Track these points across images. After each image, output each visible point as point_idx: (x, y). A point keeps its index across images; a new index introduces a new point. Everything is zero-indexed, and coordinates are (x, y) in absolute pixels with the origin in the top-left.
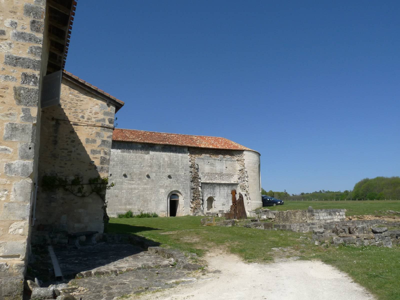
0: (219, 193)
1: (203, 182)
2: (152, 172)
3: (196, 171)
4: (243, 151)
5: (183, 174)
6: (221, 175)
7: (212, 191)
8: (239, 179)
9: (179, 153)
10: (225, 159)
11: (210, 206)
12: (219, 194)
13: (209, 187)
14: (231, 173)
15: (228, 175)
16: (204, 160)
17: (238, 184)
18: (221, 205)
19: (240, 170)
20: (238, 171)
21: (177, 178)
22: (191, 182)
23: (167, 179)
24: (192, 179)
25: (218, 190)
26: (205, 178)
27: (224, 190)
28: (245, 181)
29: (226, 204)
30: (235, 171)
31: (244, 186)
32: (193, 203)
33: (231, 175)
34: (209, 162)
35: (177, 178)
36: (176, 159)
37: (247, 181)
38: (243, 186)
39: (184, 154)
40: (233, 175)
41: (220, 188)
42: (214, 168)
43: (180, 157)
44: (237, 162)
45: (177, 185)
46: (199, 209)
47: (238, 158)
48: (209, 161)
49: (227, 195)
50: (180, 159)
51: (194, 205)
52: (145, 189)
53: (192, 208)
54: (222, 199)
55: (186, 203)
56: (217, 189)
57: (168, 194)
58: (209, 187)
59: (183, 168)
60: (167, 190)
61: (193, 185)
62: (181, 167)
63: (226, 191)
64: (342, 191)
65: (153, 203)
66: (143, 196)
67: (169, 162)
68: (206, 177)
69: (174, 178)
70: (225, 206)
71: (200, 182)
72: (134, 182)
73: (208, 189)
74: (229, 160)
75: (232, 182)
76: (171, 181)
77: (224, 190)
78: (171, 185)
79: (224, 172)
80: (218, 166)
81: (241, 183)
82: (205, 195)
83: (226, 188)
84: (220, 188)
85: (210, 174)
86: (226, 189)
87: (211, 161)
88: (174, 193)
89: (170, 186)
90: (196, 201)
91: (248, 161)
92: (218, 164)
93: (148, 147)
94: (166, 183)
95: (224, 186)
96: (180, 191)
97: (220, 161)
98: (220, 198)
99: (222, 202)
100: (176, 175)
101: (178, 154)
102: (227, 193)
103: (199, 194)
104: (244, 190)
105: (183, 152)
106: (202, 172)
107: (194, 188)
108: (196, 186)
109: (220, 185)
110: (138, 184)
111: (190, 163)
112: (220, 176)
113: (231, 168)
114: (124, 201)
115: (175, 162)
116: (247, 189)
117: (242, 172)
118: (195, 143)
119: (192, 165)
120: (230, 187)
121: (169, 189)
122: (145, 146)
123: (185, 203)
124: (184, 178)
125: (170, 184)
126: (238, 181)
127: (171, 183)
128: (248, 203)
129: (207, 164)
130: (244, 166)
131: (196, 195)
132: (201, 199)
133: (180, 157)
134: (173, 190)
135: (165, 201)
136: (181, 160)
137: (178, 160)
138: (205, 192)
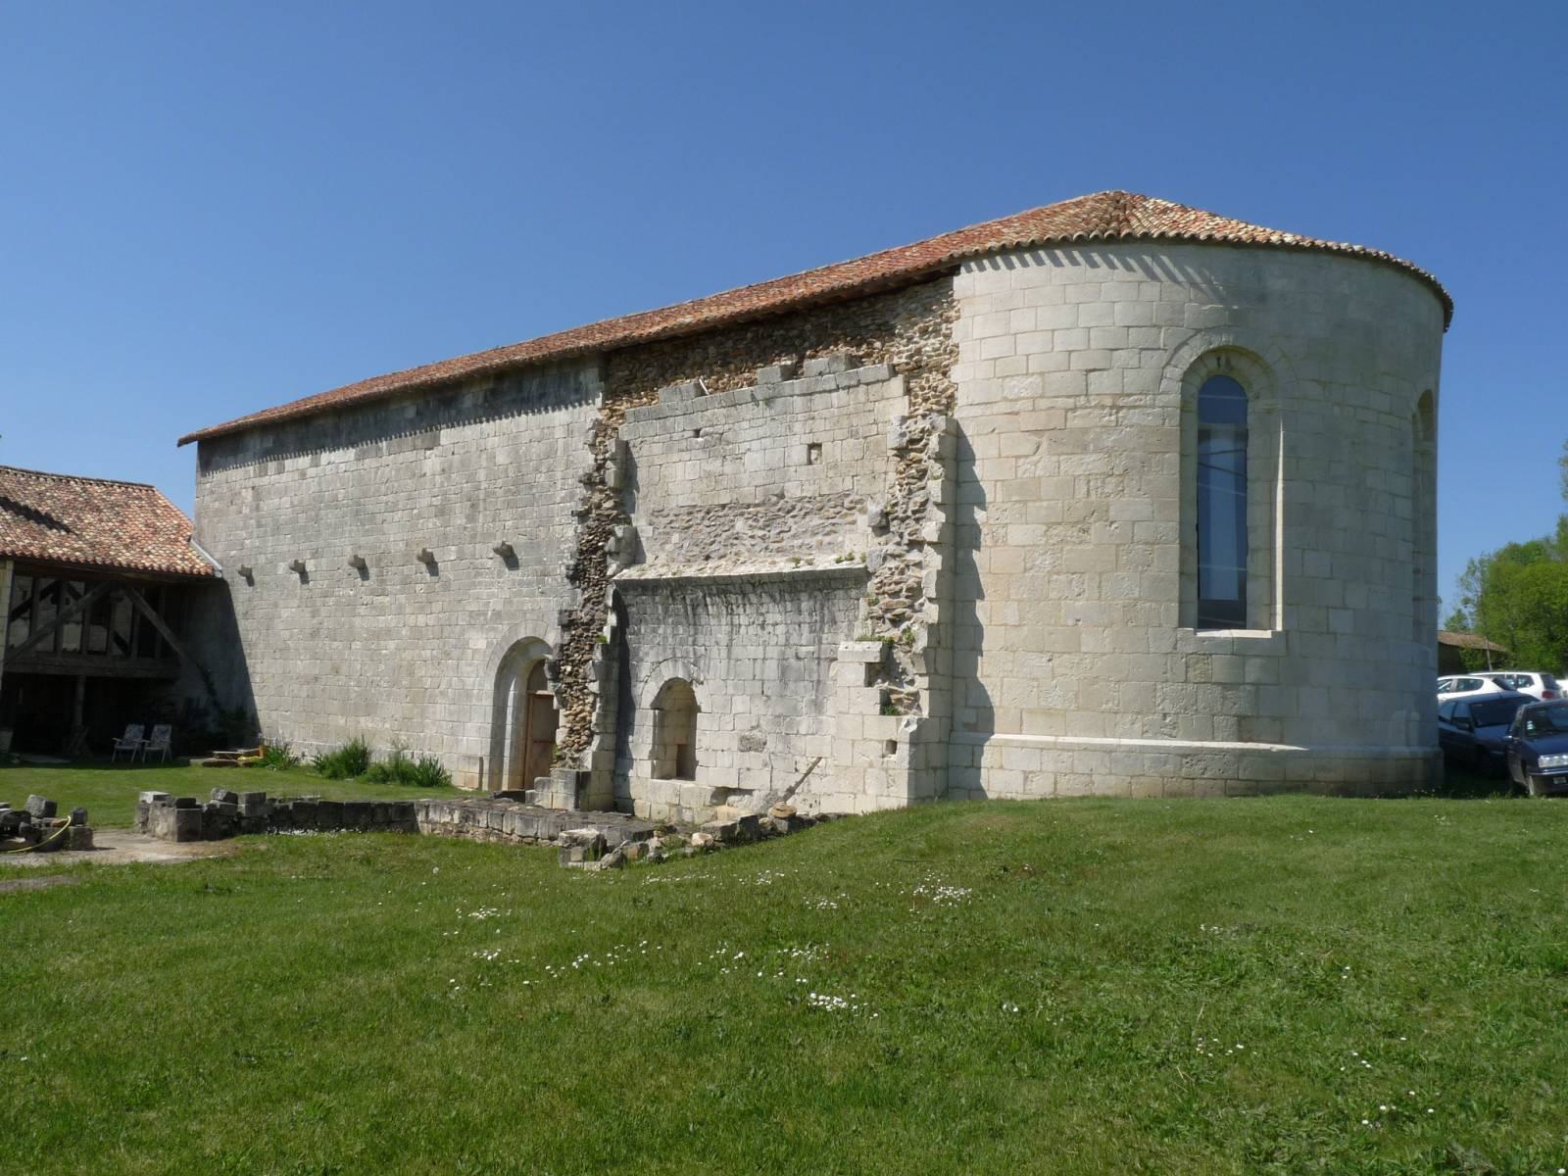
0: (724, 653)
2: (444, 540)
6: (773, 510)
9: (560, 403)
12: (725, 662)
15: (816, 505)
16: (669, 422)
18: (735, 745)
26: (668, 547)
27: (763, 626)
39: (498, 421)
49: (784, 671)
52: (417, 633)
54: (740, 704)
56: (716, 625)
60: (496, 637)
68: (675, 538)
70: (764, 756)
72: (388, 599)
77: (763, 626)
79: (793, 491)
80: (755, 445)
82: (644, 670)
83: (774, 614)
85: (711, 517)
86: (779, 618)
87: (714, 415)
92: (753, 433)
95: (754, 599)
97: (768, 401)
98: (731, 691)
99: (743, 725)
102: (783, 659)
113: (852, 441)
115: (537, 470)
118: (933, 254)
120: (806, 605)
129: (684, 444)
133: (559, 433)
134: (522, 635)
135: (484, 703)
136: (565, 450)
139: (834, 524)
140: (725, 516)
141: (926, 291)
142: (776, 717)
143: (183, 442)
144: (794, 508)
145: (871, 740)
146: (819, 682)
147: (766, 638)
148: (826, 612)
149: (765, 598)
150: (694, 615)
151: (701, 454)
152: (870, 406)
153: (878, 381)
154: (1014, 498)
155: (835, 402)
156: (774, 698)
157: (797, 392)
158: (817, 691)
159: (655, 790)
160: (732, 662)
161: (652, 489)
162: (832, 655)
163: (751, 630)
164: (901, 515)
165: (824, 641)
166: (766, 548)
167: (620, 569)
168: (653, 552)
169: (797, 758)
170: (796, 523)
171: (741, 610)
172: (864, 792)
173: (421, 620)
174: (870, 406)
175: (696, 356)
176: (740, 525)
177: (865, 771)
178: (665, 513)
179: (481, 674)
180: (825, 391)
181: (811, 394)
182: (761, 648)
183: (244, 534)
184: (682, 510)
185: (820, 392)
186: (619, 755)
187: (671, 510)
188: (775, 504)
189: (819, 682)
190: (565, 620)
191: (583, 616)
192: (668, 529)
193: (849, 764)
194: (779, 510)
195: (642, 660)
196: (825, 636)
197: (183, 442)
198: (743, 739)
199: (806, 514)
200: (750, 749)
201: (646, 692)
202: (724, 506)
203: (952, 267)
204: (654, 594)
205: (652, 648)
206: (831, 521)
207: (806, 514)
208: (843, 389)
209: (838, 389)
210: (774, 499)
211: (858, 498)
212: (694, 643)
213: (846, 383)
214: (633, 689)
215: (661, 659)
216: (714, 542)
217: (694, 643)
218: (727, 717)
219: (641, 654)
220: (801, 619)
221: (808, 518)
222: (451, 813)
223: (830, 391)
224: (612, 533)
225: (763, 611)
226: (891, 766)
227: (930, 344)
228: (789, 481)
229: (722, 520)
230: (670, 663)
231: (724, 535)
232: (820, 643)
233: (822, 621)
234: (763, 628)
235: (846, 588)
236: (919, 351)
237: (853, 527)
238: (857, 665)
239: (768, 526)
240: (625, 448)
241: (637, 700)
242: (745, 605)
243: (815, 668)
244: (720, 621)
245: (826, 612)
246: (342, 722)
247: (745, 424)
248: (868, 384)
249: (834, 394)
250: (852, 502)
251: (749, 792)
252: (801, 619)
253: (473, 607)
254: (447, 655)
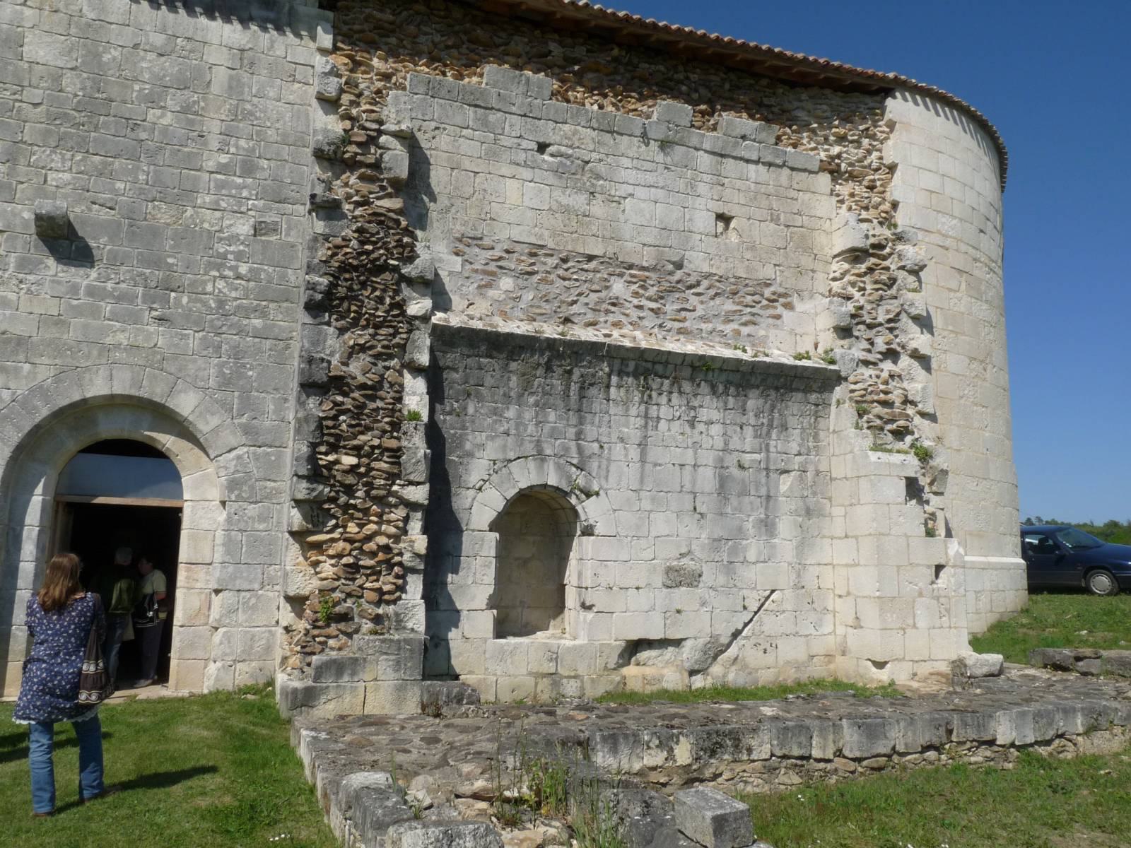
0: (634, 453)
1: (455, 320)
3: (386, 203)
4: (886, 89)
5: (243, 228)
6: (667, 280)
7: (554, 434)
8: (844, 332)
10: (709, 139)
11: (531, 595)
13: (526, 387)
14: (768, 272)
16: (493, 117)
17: (839, 379)
18: (658, 580)
19: (855, 255)
20: (839, 267)
21: (158, 263)
22: (313, 308)
23: (25, 265)
24: (324, 281)
25: (632, 428)
26: (491, 293)
27: (692, 423)
28: (905, 361)
29: (706, 569)
30: (806, 261)
31: (896, 397)
32: (318, 547)
33: (767, 292)
34: (542, 148)
35: (158, 263)
36: (170, 66)
37: (923, 360)
38: (885, 404)
40: (782, 300)
41: (647, 402)
42: (598, 208)
43: (218, 57)
44: (824, 180)
45: (161, 337)
46: (377, 619)
47: (836, 150)
48: (548, 132)
49: (723, 484)
50: (220, 77)
51: (328, 569)
53: (297, 602)
55: (245, 548)
56: (619, 417)
58: (526, 387)
59: (248, 169)
61: (333, 344)
62: (224, 159)
63: (706, 442)
64: (1100, 522)
67: (71, 84)
68: (506, 283)
69: (116, 261)
70: (700, 591)
71: (425, 318)
73: (520, 400)
74: (749, 150)
75: (780, 354)
76: (74, 289)
77: (692, 423)
78: (71, 336)
79: (698, 262)
80: (641, 192)
81: (867, 372)
82: (476, 471)
83: (710, 409)
84: (647, 402)
86: (715, 415)
88: (109, 429)
89: (57, 348)
90: (352, 528)
91: (930, 181)
95: (687, 386)
96: (185, 404)
97: (665, 145)
98: (646, 505)
99: (668, 554)
100: (155, 233)
101: (203, 20)
102: (721, 466)
103: (396, 453)
104: (899, 434)
105: (255, 11)
106: (459, 229)
107: (339, 383)
108: (364, 359)
109: (647, 368)
111: (334, 126)
112: (652, 291)
113: (772, 225)
115: (152, 101)
116: (924, 432)
117: (871, 270)
119: (346, 140)
120: (752, 403)
121: (44, 373)
123: (229, 544)
124: (243, 269)
125: (59, 322)
126: (838, 352)
127: (78, 311)
128: (939, 568)
129: (522, 156)
130: (887, 221)
131: (349, 460)
132: (412, 506)
133: (218, 57)
134: (98, 387)
136: (234, 87)
137: (193, 80)
138: (481, 437)
139: (753, 315)
140: (594, 271)
142: (714, 540)
144: (698, 284)
145: (918, 565)
146: (768, 497)
147: (697, 438)
148: (776, 415)
149: (705, 388)
150: (582, 397)
151: (551, 179)
152: (793, 194)
153: (805, 170)
154: (950, 328)
155: (752, 175)
156: (709, 516)
157: (707, 146)
158: (767, 508)
159: (501, 656)
160: (648, 467)
161: (458, 202)
162: (782, 465)
163: (676, 426)
164: (868, 321)
165: (772, 449)
166: (661, 326)
168: (462, 296)
169: (745, 592)
170: (702, 302)
171: (664, 399)
172: (914, 626)
174: (793, 194)
175: (519, 44)
176: (618, 287)
177: (914, 601)
178: (486, 242)
180: (741, 159)
181: (722, 156)
182: (690, 451)
184: (518, 248)
185: (735, 158)
186: (441, 609)
187: (499, 241)
188: (671, 273)
189: (768, 497)
192: (492, 267)
193: (896, 594)
194: (678, 282)
195: (470, 455)
196: (773, 443)
198: (669, 570)
199: (717, 294)
200: (679, 584)
201: (480, 507)
202: (590, 258)
204: (511, 357)
205: (492, 438)
206: (749, 310)
207: (717, 294)
208: (764, 164)
209: (757, 162)
210: (670, 267)
211: (781, 290)
212: (579, 436)
213: (769, 158)
214: (454, 499)
215: (511, 455)
216: (575, 302)
217: (579, 436)
218: (642, 541)
219: (468, 446)
220: (744, 420)
221: (718, 301)
222: (666, 744)
223: (748, 161)
225: (696, 404)
226: (942, 593)
228: (692, 249)
229: (591, 275)
230: (531, 464)
231: (594, 296)
232: (768, 451)
233: (771, 426)
234: (692, 425)
235: (807, 390)
237: (778, 322)
238: (897, 480)
239: (662, 298)
241: (462, 517)
242: (671, 393)
243: (763, 480)
244: (627, 410)
245: (776, 415)
247: (625, 162)
248: (792, 169)
249: (752, 167)
250: (774, 293)
251: (677, 643)
252: (744, 420)
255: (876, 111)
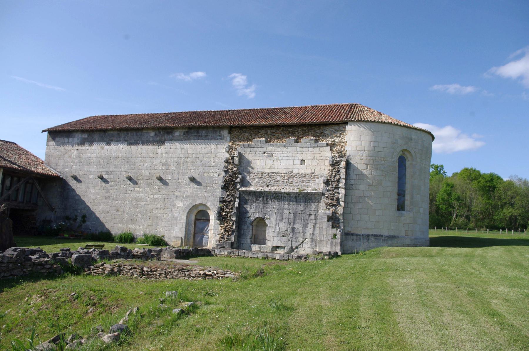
2: (166, 173)
34: (264, 153)
52: (154, 200)
56: (273, 206)
57: (187, 212)
65: (163, 223)
66: (151, 212)
68: (257, 180)
87: (269, 148)
93: (403, 126)
94: (186, 191)
110: (147, 193)
112: (286, 178)
114: (126, 217)
122: (160, 132)
134: (197, 203)
141: (336, 127)
143: (44, 131)
151: (266, 158)
167: (241, 187)
173: (156, 196)
179: (181, 213)
183: (72, 164)
190: (221, 200)
191: (228, 199)
197: (44, 131)
202: (273, 173)
203: (346, 123)
224: (238, 177)
227: (337, 140)
236: (334, 141)
240: (240, 156)
246: (120, 226)
253: (178, 194)
254: (167, 207)
255: (343, 131)
